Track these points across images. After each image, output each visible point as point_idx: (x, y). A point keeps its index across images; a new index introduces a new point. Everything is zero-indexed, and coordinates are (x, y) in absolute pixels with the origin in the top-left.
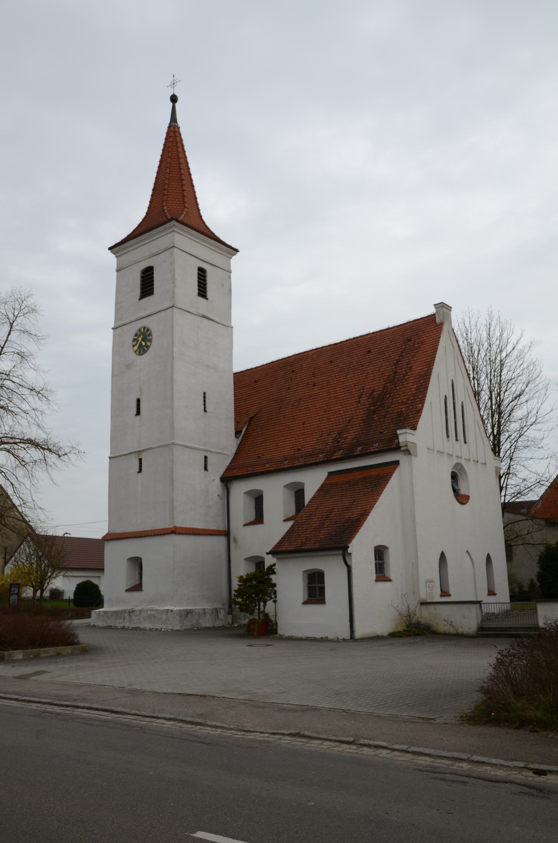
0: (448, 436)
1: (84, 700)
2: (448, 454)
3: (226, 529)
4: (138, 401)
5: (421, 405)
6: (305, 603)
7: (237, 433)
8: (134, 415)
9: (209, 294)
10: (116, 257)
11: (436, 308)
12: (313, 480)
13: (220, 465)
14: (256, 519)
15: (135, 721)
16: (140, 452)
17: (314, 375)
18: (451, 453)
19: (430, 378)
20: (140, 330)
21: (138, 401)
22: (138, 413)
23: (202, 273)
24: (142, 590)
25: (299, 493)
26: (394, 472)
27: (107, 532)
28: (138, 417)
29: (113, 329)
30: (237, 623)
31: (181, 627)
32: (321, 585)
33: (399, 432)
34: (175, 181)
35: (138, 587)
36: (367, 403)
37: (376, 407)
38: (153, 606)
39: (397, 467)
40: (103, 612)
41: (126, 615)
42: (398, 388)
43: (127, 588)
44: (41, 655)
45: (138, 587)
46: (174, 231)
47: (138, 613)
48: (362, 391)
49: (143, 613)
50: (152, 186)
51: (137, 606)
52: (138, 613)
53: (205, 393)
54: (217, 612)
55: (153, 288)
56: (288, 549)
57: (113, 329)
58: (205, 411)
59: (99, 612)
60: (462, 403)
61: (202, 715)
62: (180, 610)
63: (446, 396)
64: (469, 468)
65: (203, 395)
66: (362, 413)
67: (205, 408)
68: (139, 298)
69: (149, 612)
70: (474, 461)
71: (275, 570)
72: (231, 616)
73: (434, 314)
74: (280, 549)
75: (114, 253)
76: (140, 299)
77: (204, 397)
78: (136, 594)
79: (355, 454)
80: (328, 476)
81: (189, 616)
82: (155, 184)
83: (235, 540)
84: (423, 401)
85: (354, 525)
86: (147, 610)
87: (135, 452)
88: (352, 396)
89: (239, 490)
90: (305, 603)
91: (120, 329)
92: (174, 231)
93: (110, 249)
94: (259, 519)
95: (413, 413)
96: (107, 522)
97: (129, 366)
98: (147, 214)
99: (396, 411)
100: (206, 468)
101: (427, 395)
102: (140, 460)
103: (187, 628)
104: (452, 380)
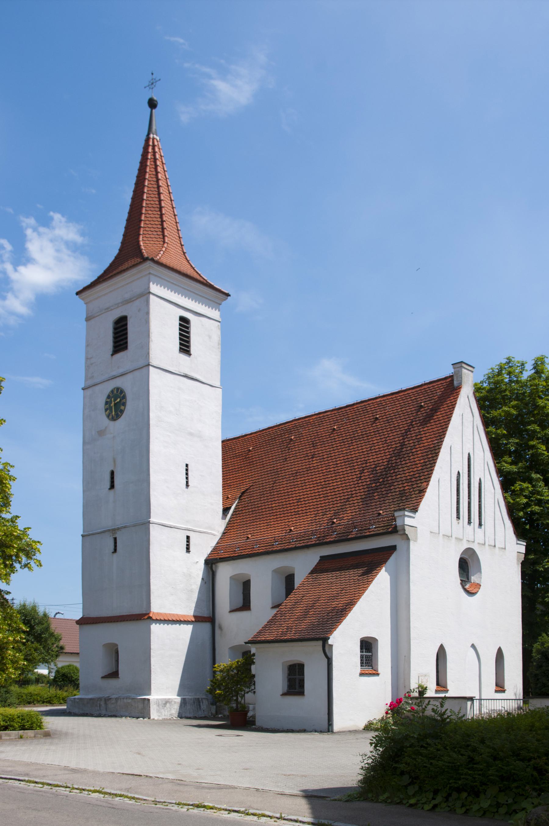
0: (458, 518)
1: (27, 775)
2: (456, 538)
3: (211, 616)
4: (112, 473)
5: (425, 484)
6: (284, 694)
7: (226, 510)
8: (107, 489)
9: (193, 349)
10: (86, 304)
11: (454, 368)
12: (302, 564)
13: (204, 547)
14: (243, 605)
15: (65, 792)
16: (114, 531)
17: (314, 445)
18: (461, 537)
19: (439, 452)
20: (112, 391)
21: (112, 473)
22: (112, 486)
23: (184, 323)
24: (118, 677)
25: (289, 580)
26: (389, 558)
27: (81, 616)
28: (112, 491)
29: (83, 389)
30: (221, 714)
31: (159, 716)
32: (302, 677)
33: (396, 514)
34: (152, 209)
35: (114, 674)
36: (368, 480)
37: (378, 484)
38: (130, 695)
39: (392, 553)
40: (78, 699)
41: (102, 703)
42: (403, 462)
43: (103, 675)
44: (3, 738)
45: (114, 674)
46: (150, 273)
47: (114, 701)
48: (364, 465)
49: (119, 702)
50: (126, 216)
51: (114, 694)
52: (114, 701)
53: (187, 465)
54: (199, 702)
55: (127, 343)
56: (267, 639)
57: (83, 389)
58: (187, 485)
59: (75, 698)
60: (480, 480)
61: (128, 790)
62: (157, 699)
63: (459, 473)
64: (483, 555)
65: (185, 468)
66: (362, 490)
67: (187, 482)
68: (111, 353)
69: (125, 701)
70: (489, 545)
71: (254, 661)
72: (215, 707)
73: (452, 377)
74: (259, 639)
75: (83, 299)
76: (112, 355)
77: (187, 470)
78: (113, 682)
79: (350, 537)
80: (320, 560)
81: (168, 705)
82: (130, 213)
83: (220, 628)
84: (427, 479)
85: (341, 613)
86: (123, 698)
87: (109, 530)
88: (353, 471)
89: (225, 572)
90: (284, 694)
91: (91, 389)
92: (150, 273)
93: (77, 294)
94: (246, 606)
95: (416, 493)
96: (81, 606)
97: (101, 433)
98: (120, 250)
99: (398, 490)
100: (188, 549)
101: (434, 472)
102: (115, 539)
103: (165, 717)
104: (469, 454)
